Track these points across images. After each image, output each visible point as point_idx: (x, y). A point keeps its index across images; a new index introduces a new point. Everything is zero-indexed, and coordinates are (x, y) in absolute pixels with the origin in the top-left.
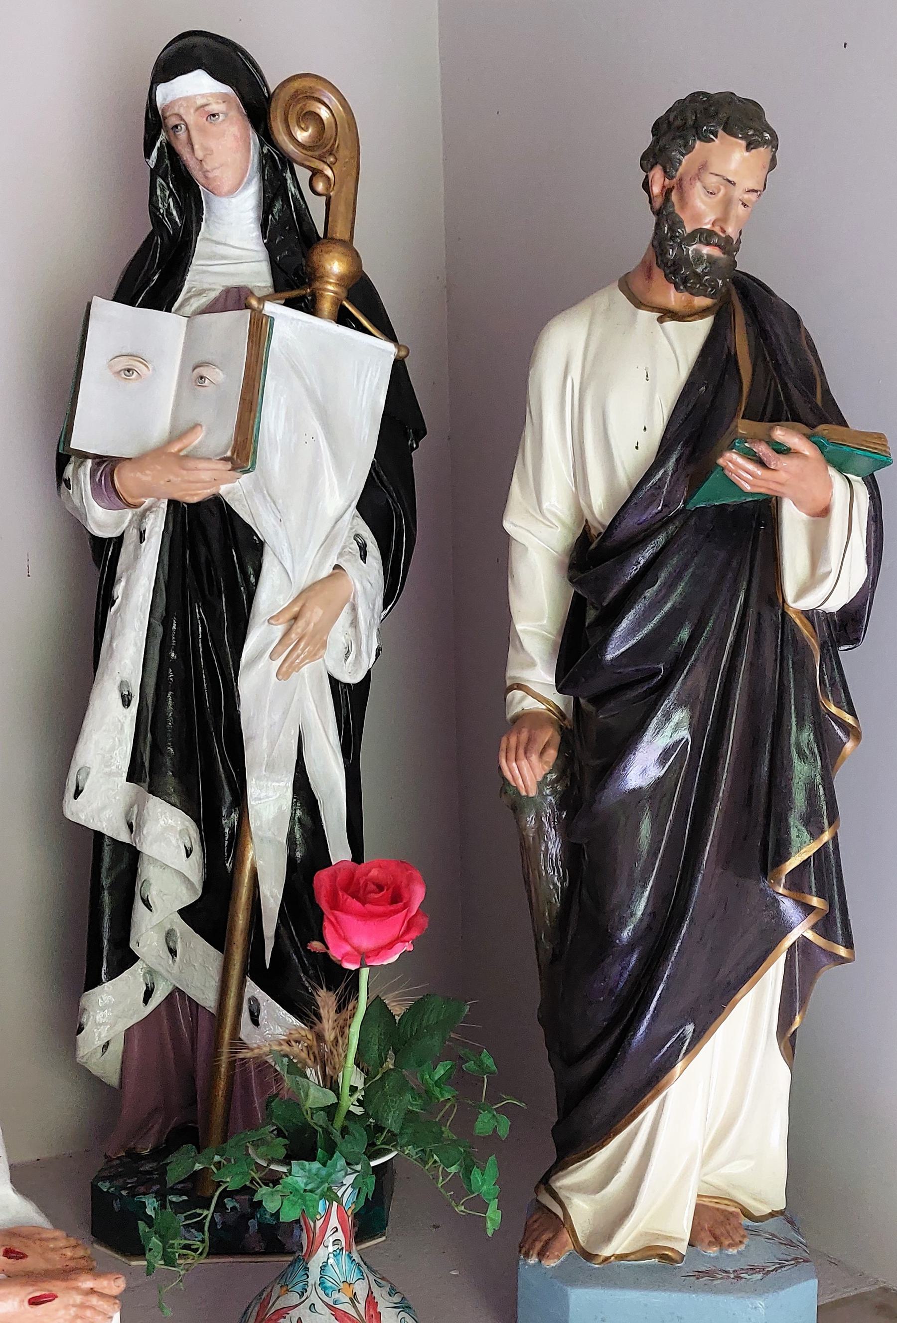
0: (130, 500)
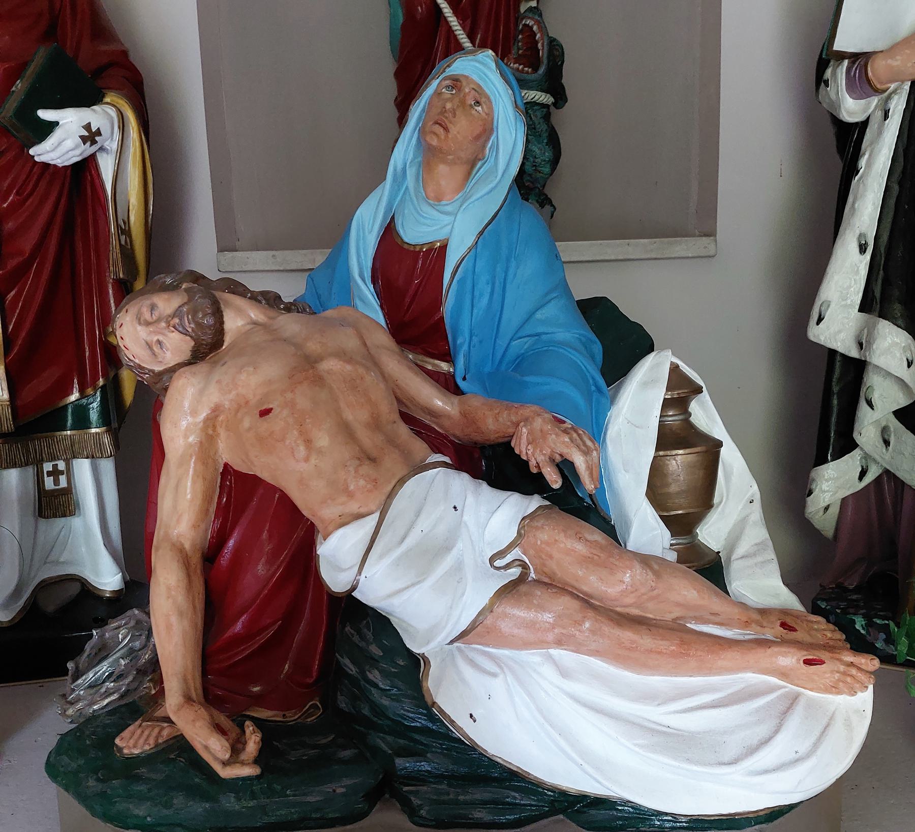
0: (878, 86)
